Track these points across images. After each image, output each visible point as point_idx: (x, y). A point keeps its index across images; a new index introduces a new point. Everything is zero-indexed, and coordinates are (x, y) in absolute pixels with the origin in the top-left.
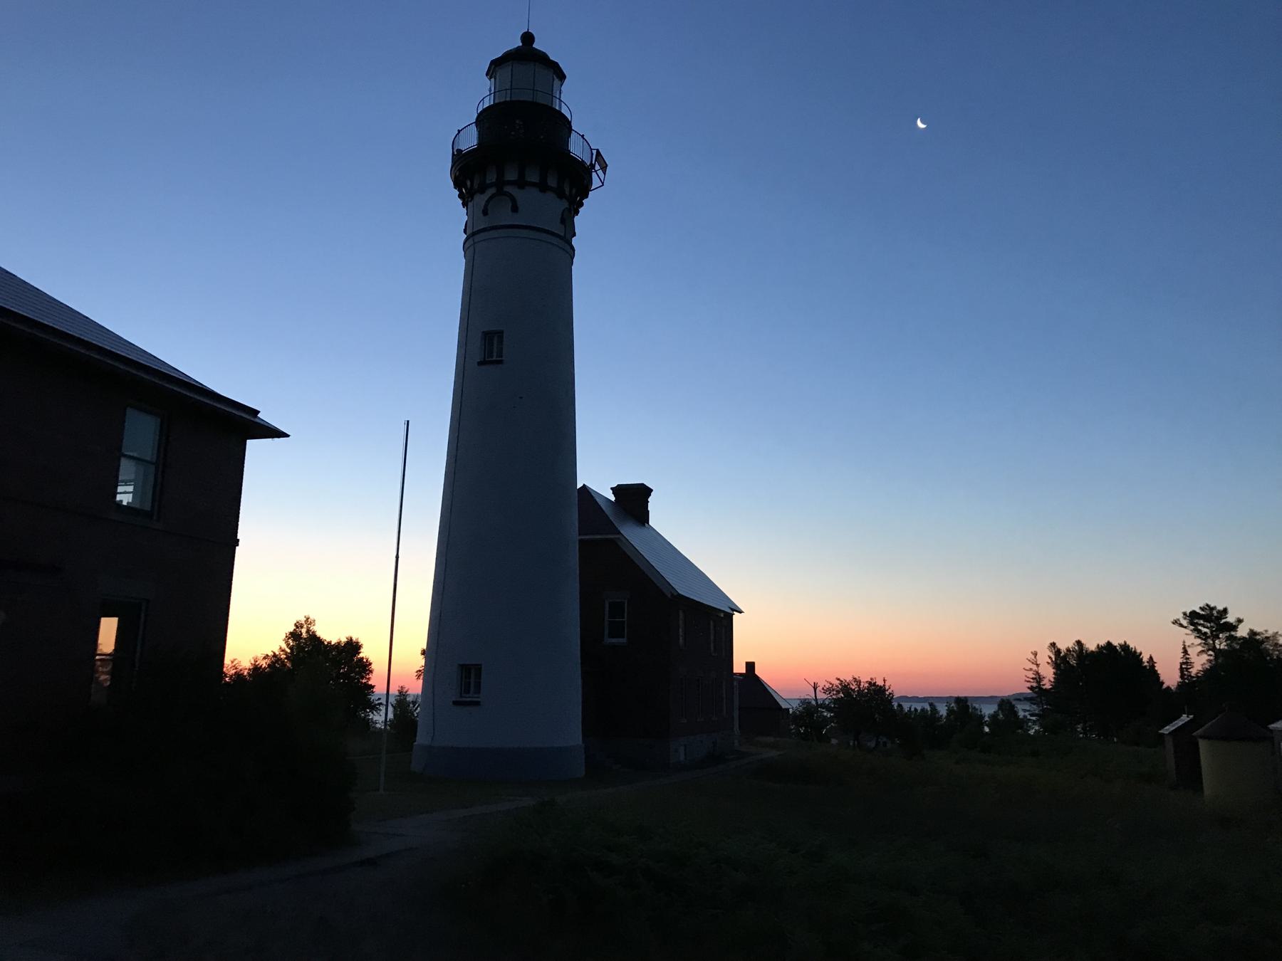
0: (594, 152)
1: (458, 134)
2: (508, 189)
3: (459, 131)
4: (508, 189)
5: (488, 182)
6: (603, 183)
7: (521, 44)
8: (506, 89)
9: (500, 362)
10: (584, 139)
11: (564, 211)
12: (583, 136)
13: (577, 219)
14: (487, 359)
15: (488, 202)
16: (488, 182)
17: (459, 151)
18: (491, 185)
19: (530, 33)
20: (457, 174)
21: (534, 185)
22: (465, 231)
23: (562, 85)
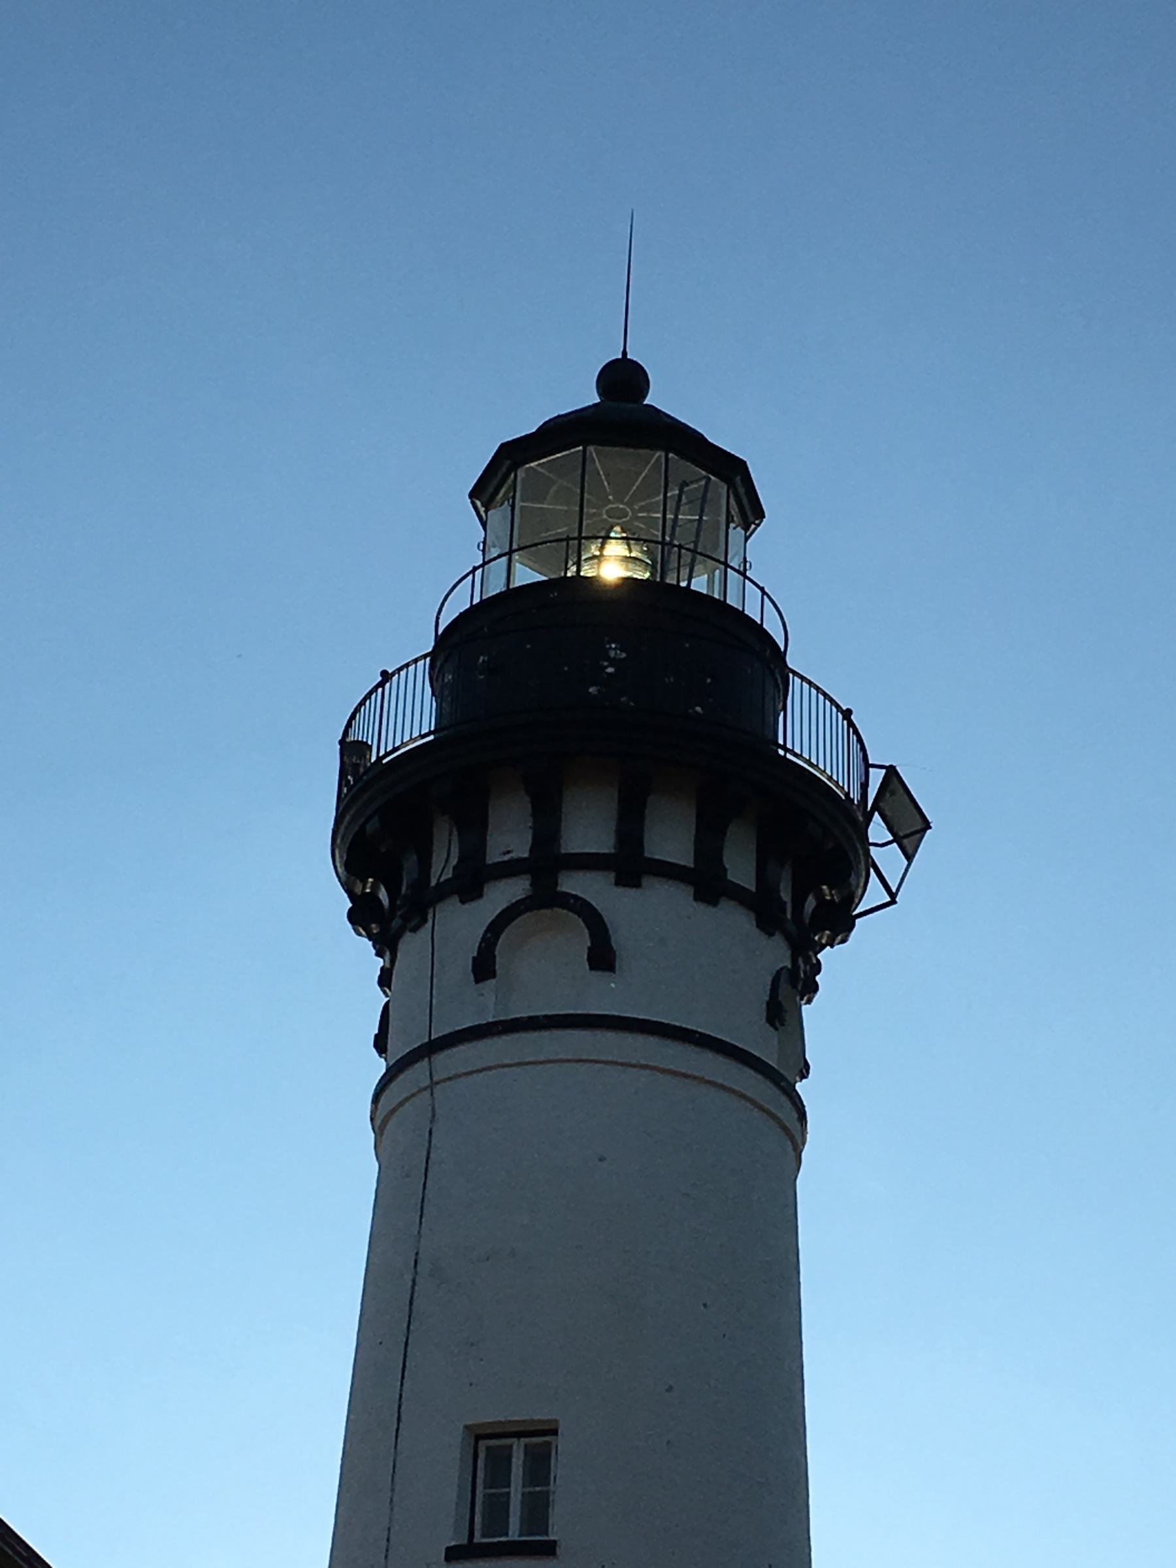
0: (876, 778)
1: (381, 684)
2: (572, 884)
3: (386, 676)
4: (572, 884)
5: (494, 856)
6: (893, 896)
7: (598, 400)
8: (568, 539)
9: (548, 1549)
10: (851, 724)
11: (779, 973)
12: (847, 714)
13: (807, 1011)
14: (478, 1539)
15: (495, 929)
16: (494, 856)
17: (363, 748)
18: (509, 869)
19: (631, 361)
20: (373, 826)
21: (668, 871)
22: (380, 1044)
23: (747, 539)
